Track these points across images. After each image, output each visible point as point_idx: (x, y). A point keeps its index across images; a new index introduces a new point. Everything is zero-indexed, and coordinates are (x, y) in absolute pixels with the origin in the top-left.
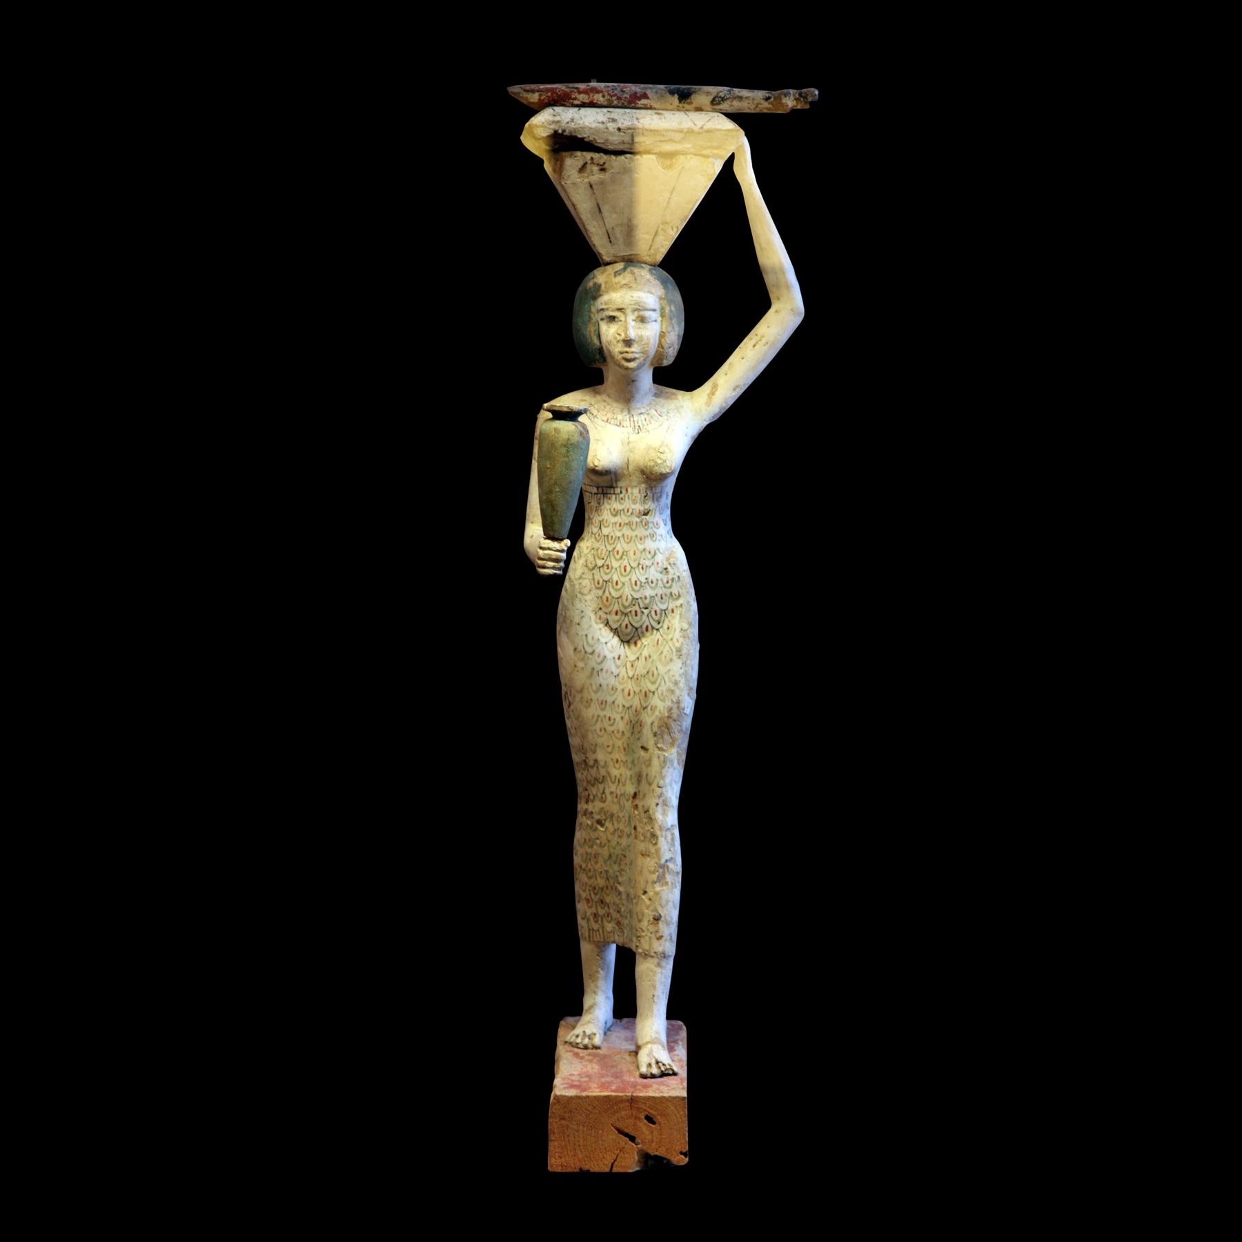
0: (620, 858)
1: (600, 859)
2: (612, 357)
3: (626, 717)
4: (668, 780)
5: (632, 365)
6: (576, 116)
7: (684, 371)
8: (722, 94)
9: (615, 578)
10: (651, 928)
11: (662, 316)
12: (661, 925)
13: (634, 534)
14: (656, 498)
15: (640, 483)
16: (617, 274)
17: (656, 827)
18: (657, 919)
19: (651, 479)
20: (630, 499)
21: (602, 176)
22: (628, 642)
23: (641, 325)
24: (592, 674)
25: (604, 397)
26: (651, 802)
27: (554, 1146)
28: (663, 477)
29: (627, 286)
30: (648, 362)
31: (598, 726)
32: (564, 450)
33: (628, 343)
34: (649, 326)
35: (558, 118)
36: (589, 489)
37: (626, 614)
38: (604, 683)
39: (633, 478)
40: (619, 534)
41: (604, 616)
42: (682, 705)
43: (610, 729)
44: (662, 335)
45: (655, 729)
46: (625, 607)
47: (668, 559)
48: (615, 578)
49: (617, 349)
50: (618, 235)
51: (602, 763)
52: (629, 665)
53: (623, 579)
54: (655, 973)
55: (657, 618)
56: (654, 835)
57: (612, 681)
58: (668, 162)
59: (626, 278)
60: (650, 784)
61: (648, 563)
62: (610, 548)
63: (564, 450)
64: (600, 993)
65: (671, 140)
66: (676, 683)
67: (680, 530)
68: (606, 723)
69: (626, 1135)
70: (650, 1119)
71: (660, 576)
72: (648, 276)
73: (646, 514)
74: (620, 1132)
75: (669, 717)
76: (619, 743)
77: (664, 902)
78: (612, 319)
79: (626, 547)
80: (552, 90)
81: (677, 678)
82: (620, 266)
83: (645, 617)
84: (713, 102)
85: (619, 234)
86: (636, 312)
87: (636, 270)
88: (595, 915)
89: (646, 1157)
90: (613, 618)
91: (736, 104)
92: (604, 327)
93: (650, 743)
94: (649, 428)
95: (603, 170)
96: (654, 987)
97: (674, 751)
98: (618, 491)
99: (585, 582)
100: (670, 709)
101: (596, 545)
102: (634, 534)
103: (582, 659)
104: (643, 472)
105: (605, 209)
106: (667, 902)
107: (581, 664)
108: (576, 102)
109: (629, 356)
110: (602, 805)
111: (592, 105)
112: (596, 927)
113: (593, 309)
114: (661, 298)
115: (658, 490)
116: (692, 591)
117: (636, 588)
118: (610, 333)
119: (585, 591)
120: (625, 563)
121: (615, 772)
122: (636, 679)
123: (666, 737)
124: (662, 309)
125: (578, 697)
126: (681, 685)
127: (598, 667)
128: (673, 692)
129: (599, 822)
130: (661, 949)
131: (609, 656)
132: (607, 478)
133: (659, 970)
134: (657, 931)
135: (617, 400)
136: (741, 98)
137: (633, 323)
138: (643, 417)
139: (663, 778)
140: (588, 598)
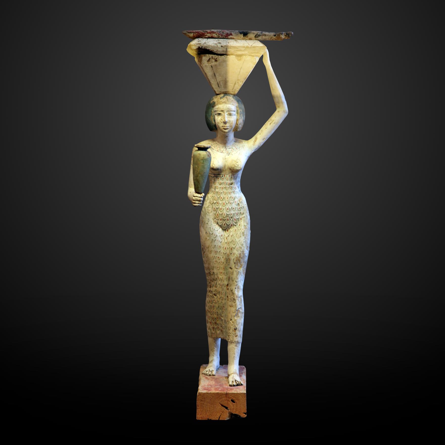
0: (222, 308)
1: (215, 308)
2: (219, 128)
3: (224, 257)
4: (239, 279)
5: (226, 131)
6: (207, 42)
7: (245, 133)
8: (259, 34)
9: (220, 207)
10: (233, 332)
11: (237, 113)
12: (237, 331)
13: (227, 191)
14: (235, 178)
15: (229, 173)
16: (221, 98)
17: (235, 296)
18: (235, 329)
19: (233, 172)
20: (226, 179)
21: (216, 63)
22: (225, 230)
23: (230, 116)
24: (212, 241)
25: (217, 142)
26: (233, 287)
27: (198, 411)
28: (238, 171)
29: (225, 102)
30: (232, 130)
31: (214, 260)
32: (202, 161)
33: (225, 123)
34: (233, 117)
35: (200, 42)
36: (211, 175)
37: (224, 220)
38: (216, 245)
39: (227, 171)
40: (222, 191)
41: (217, 221)
42: (244, 253)
43: (218, 261)
44: (237, 120)
45: (235, 261)
46: (224, 218)
47: (239, 200)
48: (220, 207)
49: (221, 125)
50: (222, 84)
51: (216, 274)
52: (225, 238)
53: (223, 208)
54: (235, 348)
55: (235, 221)
56: (234, 299)
57: (219, 244)
58: (239, 58)
59: (224, 100)
60: (233, 281)
61: (232, 202)
62: (218, 196)
63: (202, 161)
64: (215, 356)
65: (241, 50)
66: (242, 245)
67: (243, 190)
68: (217, 259)
69: (224, 407)
70: (233, 401)
71: (236, 206)
72: (232, 99)
73: (231, 184)
74: (222, 406)
75: (240, 257)
76: (222, 266)
77: (238, 323)
78: (219, 114)
79: (224, 196)
80: (198, 32)
81: (243, 243)
82: (222, 95)
83: (231, 221)
84: (255, 37)
85: (222, 84)
86: (228, 112)
87: (228, 97)
88: (213, 328)
89: (231, 415)
90: (220, 222)
91: (264, 37)
92: (216, 117)
93: (233, 266)
94: (233, 153)
95: (216, 61)
96: (234, 354)
97: (242, 269)
98: (221, 176)
99: (210, 209)
100: (240, 254)
101: (214, 195)
102: (227, 191)
103: (209, 236)
104: (230, 169)
105: (217, 75)
106: (239, 323)
107: (208, 238)
108: (206, 37)
109: (225, 128)
110: (216, 288)
111: (212, 38)
112: (213, 332)
113: (213, 111)
114: (237, 107)
115: (236, 175)
116: (248, 212)
117: (228, 211)
118: (218, 119)
119: (210, 212)
120: (224, 202)
121: (220, 277)
122: (228, 243)
123: (239, 264)
124: (237, 111)
125: (207, 250)
126: (244, 245)
127: (214, 239)
128: (241, 248)
129: (215, 295)
130: (237, 340)
131: (218, 235)
132: (218, 171)
133: (236, 348)
134: (235, 334)
135: (221, 143)
136: (265, 35)
137: (227, 116)
138: (230, 149)
139: (237, 279)
140: (211, 214)
